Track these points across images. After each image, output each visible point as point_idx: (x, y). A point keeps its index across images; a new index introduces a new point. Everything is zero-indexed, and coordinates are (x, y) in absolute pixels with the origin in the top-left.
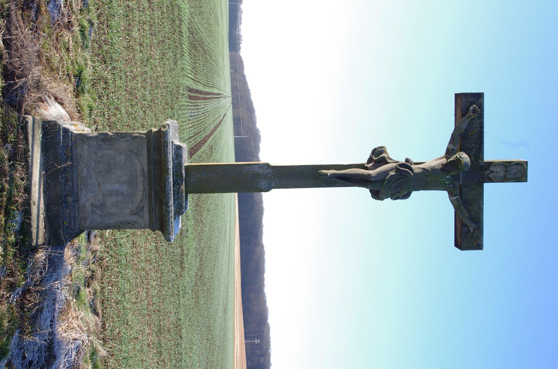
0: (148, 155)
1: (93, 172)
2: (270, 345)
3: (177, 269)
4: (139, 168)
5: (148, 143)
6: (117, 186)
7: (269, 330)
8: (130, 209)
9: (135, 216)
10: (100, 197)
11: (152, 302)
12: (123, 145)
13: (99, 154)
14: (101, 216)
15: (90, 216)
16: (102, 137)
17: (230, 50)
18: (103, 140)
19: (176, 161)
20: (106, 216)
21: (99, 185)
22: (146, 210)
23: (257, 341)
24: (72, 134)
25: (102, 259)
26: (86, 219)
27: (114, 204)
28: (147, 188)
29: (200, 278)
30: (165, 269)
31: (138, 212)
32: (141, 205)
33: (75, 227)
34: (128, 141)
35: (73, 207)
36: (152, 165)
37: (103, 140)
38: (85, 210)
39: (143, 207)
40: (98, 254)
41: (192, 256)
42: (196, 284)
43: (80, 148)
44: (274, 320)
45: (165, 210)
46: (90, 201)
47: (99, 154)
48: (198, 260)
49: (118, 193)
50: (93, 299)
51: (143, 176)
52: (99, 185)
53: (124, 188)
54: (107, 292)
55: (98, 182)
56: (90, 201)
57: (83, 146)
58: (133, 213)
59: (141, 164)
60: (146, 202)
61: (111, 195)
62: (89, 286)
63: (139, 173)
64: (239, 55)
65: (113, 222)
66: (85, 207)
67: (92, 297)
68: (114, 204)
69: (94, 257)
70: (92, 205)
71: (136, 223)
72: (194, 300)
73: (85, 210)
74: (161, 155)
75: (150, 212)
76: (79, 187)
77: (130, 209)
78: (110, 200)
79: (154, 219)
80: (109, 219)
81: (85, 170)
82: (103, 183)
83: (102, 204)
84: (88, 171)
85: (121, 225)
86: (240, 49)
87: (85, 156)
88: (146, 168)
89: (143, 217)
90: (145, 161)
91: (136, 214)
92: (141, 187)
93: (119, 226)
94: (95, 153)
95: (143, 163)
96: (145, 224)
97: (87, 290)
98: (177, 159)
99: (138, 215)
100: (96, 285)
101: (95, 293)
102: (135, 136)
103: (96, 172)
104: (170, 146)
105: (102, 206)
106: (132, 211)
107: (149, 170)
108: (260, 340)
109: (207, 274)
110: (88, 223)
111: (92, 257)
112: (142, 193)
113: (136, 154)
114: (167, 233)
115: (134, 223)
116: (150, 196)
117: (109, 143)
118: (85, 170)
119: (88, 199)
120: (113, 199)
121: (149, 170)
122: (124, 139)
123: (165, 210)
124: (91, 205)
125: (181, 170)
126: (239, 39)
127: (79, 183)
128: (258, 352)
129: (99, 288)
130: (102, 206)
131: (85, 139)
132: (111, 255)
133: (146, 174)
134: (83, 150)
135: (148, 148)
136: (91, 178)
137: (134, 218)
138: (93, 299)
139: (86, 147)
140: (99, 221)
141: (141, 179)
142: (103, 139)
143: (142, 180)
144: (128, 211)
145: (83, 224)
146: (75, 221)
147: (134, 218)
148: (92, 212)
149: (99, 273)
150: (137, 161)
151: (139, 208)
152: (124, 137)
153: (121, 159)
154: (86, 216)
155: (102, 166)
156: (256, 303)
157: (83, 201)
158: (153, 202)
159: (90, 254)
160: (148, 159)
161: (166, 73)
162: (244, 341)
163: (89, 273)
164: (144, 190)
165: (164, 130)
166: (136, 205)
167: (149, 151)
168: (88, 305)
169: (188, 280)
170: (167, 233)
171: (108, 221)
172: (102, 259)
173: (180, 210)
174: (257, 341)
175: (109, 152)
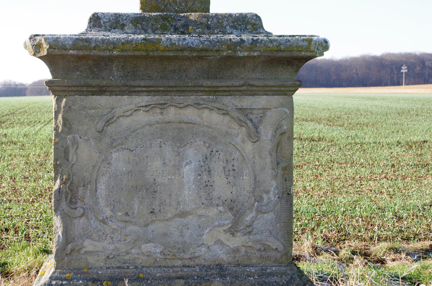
0: (112, 93)
1: (151, 227)
2: (410, 54)
3: (323, 144)
4: (142, 117)
5: (81, 93)
6: (188, 172)
7: (389, 55)
8: (243, 142)
9: (262, 128)
10: (213, 212)
11: (380, 175)
12: (85, 154)
13: (108, 212)
14: (259, 211)
15: (258, 237)
16: (64, 205)
17: (25, 95)
18: (72, 202)
19: (129, 27)
20: (260, 199)
21: (183, 214)
22: (247, 102)
23: (404, 70)
24: (56, 279)
25: (327, 239)
26: (267, 248)
27: (231, 179)
28: (192, 99)
29: (331, 121)
30: (325, 159)
31: (251, 122)
32: (235, 114)
33: (285, 273)
34: (75, 142)
35: (237, 277)
36: (138, 83)
37: (72, 202)
38: (243, 250)
39: (241, 110)
40: (319, 243)
41: (302, 129)
42: (340, 126)
43: (91, 260)
44: (377, 49)
45: (250, 50)
46: (223, 237)
47: (108, 212)
48: (304, 123)
49: (205, 168)
50: (407, 254)
51: (163, 106)
52: (183, 214)
53: (193, 154)
54: (385, 233)
55: (175, 216)
56: (223, 237)
57: (86, 252)
58: (254, 135)
59: (133, 112)
60: (230, 102)
61: (208, 186)
62: (382, 262)
63: (155, 116)
64: (31, 85)
65: (274, 184)
66: (236, 251)
67: (403, 255)
68: (231, 179)
69: (326, 251)
70: (232, 231)
71: (278, 127)
72: (365, 127)
73: (243, 250)
74: (111, 59)
75: (251, 91)
76: (187, 263)
77: (243, 142)
78: (222, 187)
79: (271, 83)
80: (268, 192)
81: (147, 247)
82: (178, 203)
83: (231, 209)
84: (149, 241)
85: (283, 164)
86: (22, 85)
87: (112, 247)
88: (143, 100)
89: (265, 110)
90: (126, 102)
91: (256, 128)
92: (190, 114)
93: (285, 169)
94: (104, 222)
95: (133, 106)
96: (282, 106)
97: (390, 264)
98: (123, 25)
99: (260, 122)
100: (379, 249)
101: (397, 251)
102: (64, 125)
103: (152, 221)
104: (89, 36)
105: (235, 208)
106: (249, 136)
107: (150, 91)
108: (403, 66)
109: (325, 114)
110: (275, 244)
111: (327, 255)
112: (206, 112)
113: (108, 122)
114: (308, 49)
115: (279, 132)
116: (215, 91)
117: (81, 189)
118: (147, 247)
119: (219, 242)
120: (220, 181)
121: (149, 93)
122: (72, 151)
123: (250, 50)
124: (233, 234)
125: (151, 18)
126: (10, 85)
127: (179, 263)
128: (418, 68)
129: (384, 245)
130: (235, 208)
131: (69, 247)
132: (318, 225)
133: (157, 99)
134: (99, 250)
135: (93, 93)
136: (165, 235)
137: (267, 133)
138: (407, 254)
139: (89, 245)
140: (270, 216)
141: (172, 114)
142: (71, 202)
143: (172, 110)
144: (249, 147)
145: (279, 255)
146: (271, 274)
147: (267, 133)
148: (250, 233)
149: (355, 244)
150: (125, 122)
151: (242, 118)
152: (66, 152)
153: (119, 160)
154: (258, 247)
155: (136, 206)
156: (354, 71)
157: (222, 255)
158: (229, 83)
159: (321, 257)
160: (122, 93)
161: (23, 153)
162: (404, 86)
163: (358, 260)
164: (197, 105)
165: (45, 46)
166: (235, 125)
167: (101, 91)
168: (423, 262)
169: (336, 133)
170: (308, 49)
171: (271, 195)
172: (327, 239)
173: (248, 23)
174: (404, 70)
175: (102, 189)
